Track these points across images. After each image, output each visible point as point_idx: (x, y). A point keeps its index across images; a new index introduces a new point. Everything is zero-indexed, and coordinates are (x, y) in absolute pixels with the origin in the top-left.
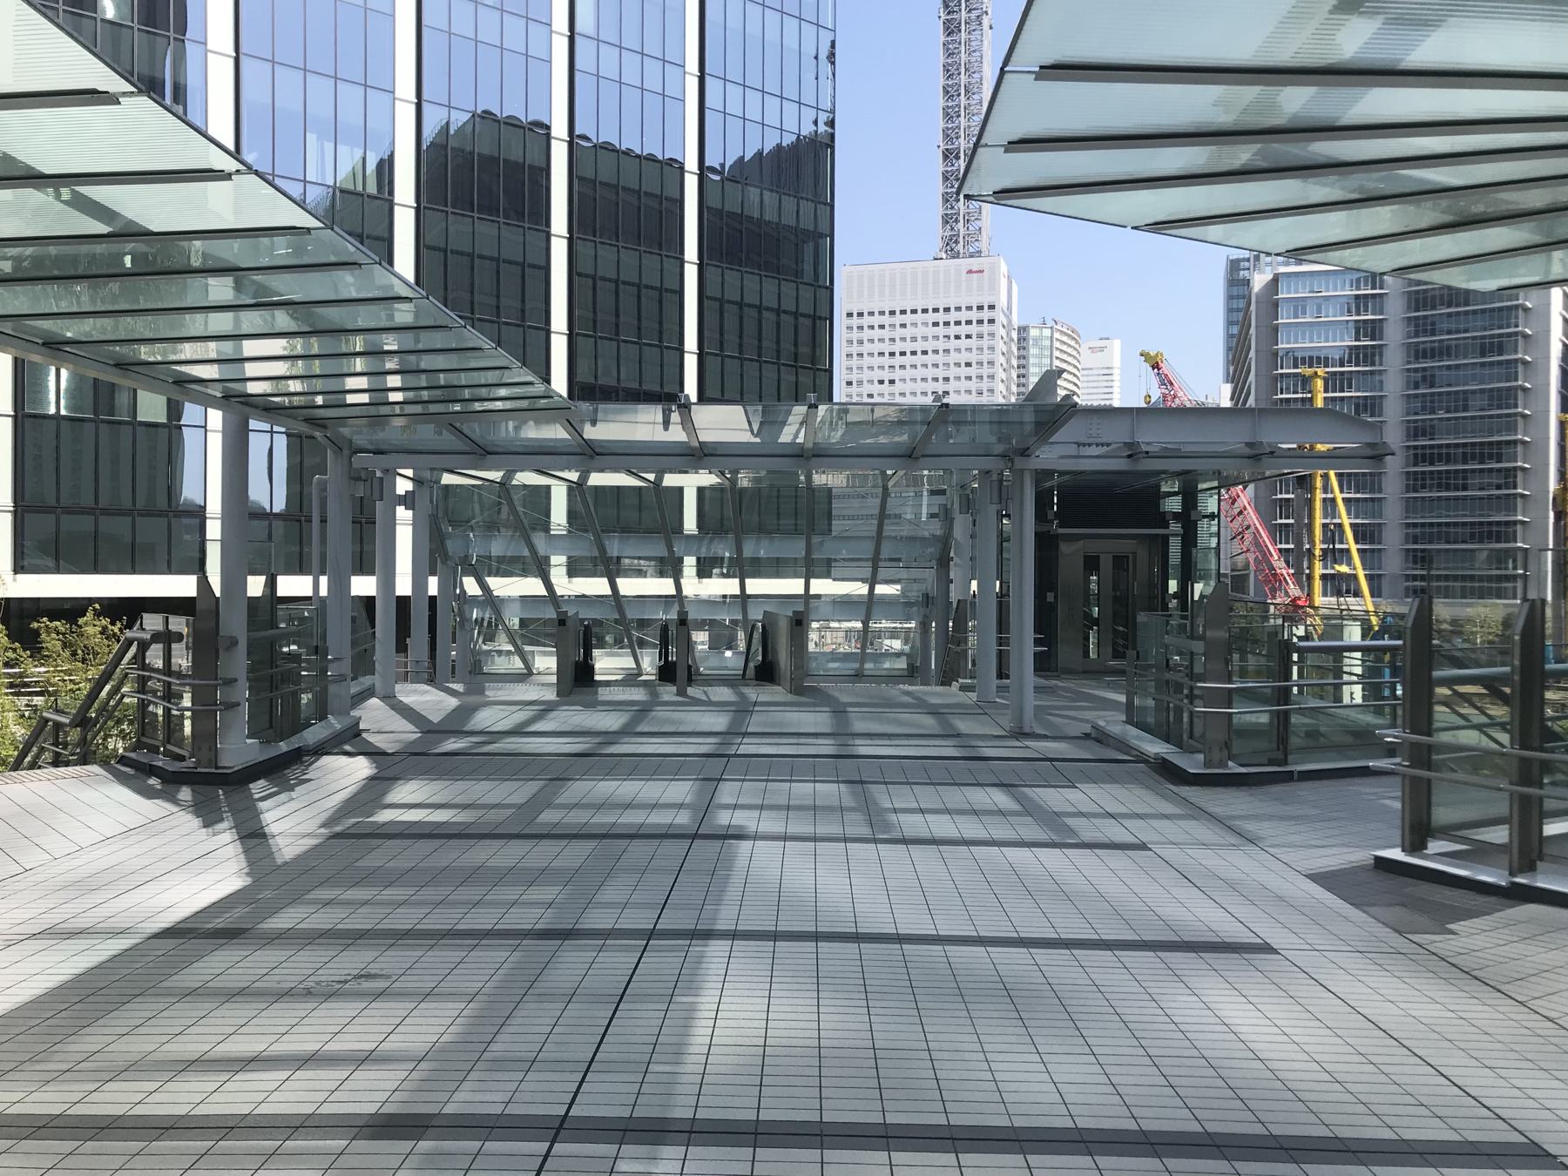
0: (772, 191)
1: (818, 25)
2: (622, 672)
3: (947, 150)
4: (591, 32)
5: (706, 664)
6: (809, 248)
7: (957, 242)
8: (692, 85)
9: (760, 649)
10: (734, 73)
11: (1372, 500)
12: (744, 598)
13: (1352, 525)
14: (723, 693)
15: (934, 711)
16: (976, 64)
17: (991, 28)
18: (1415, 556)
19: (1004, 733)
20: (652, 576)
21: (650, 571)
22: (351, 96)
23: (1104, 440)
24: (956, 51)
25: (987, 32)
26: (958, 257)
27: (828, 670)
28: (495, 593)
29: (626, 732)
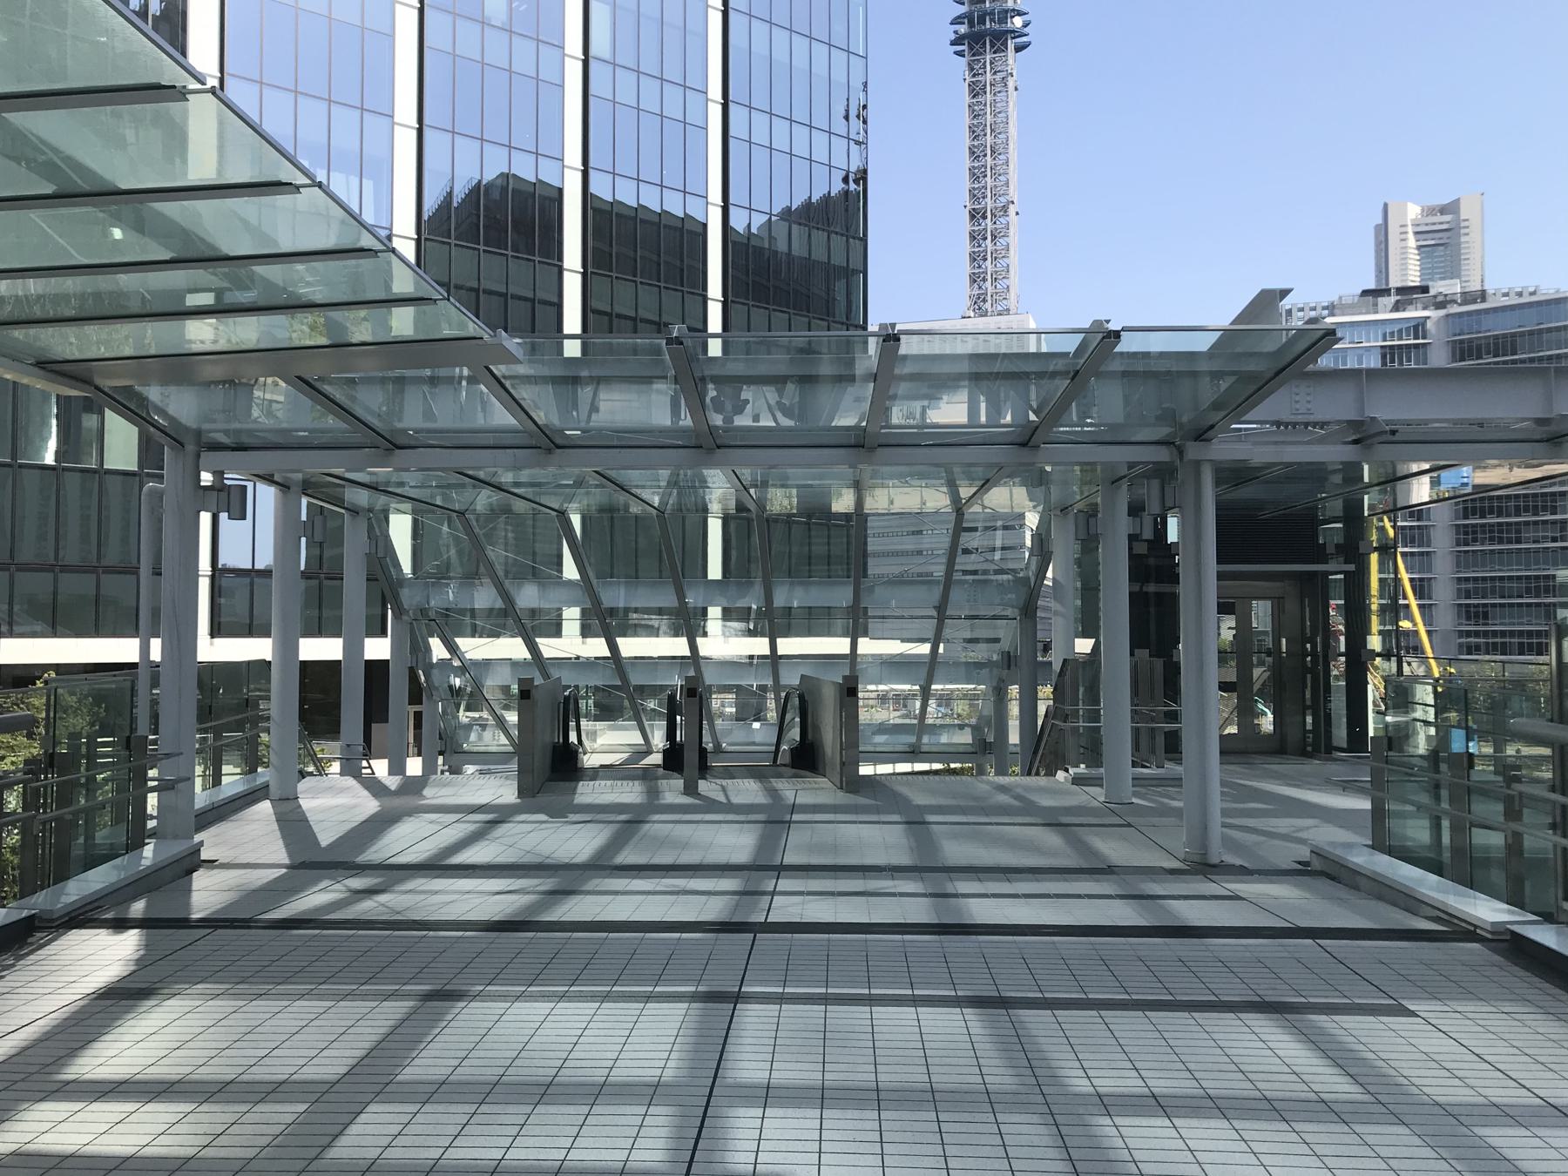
0: (800, 224)
1: (848, 51)
2: (627, 749)
3: (974, 209)
4: (607, 55)
5: (729, 739)
6: (840, 286)
7: (984, 301)
8: (715, 112)
9: (798, 720)
10: (760, 101)
11: (1422, 554)
12: (774, 659)
13: (1411, 580)
14: (747, 791)
15: (1053, 820)
16: (1002, 125)
17: (1016, 89)
18: (1468, 612)
19: (1176, 864)
20: (666, 634)
21: (664, 628)
22: (346, 120)
23: (1319, 417)
24: (981, 113)
25: (1013, 94)
26: (986, 315)
27: (876, 745)
28: (468, 656)
29: (601, 865)
